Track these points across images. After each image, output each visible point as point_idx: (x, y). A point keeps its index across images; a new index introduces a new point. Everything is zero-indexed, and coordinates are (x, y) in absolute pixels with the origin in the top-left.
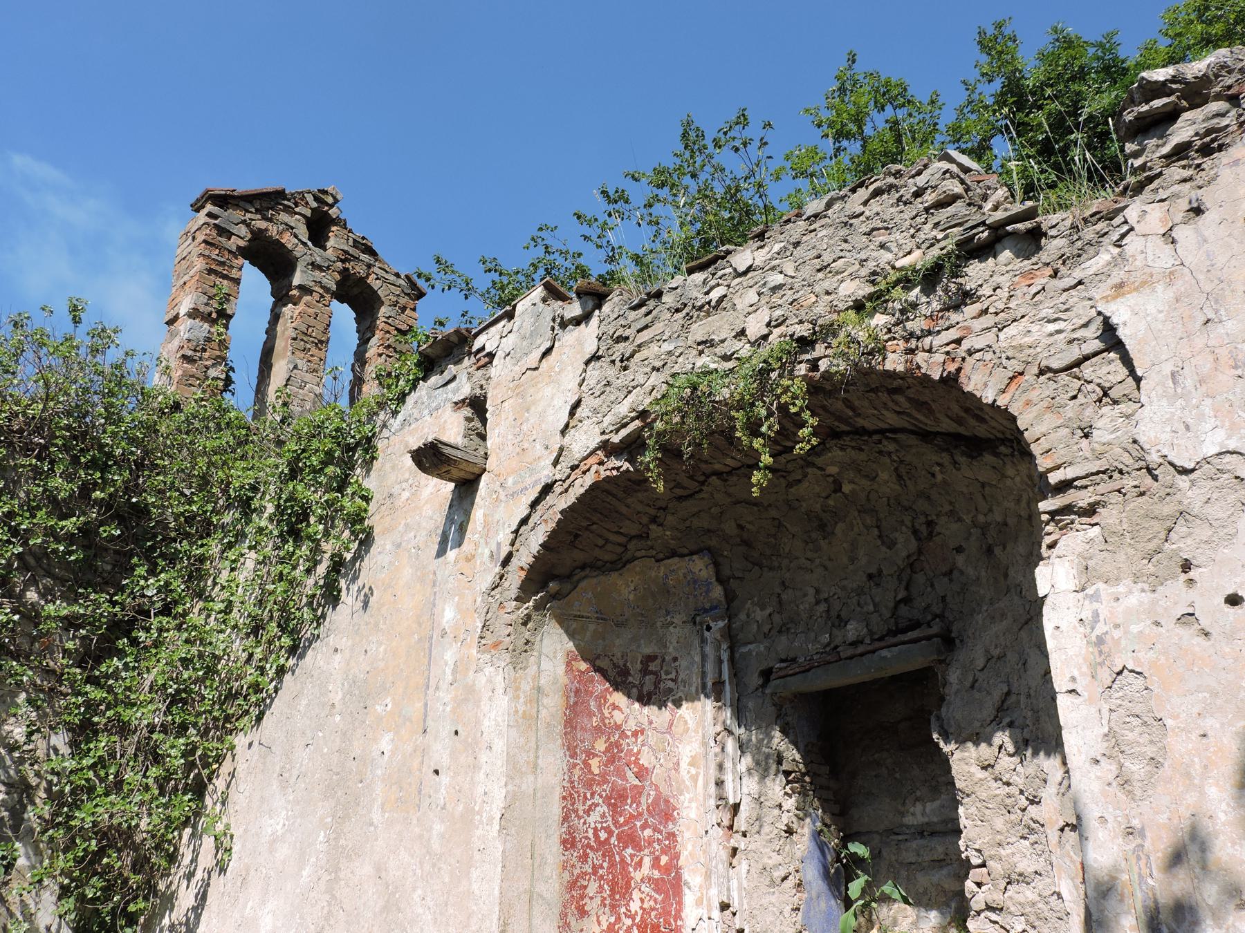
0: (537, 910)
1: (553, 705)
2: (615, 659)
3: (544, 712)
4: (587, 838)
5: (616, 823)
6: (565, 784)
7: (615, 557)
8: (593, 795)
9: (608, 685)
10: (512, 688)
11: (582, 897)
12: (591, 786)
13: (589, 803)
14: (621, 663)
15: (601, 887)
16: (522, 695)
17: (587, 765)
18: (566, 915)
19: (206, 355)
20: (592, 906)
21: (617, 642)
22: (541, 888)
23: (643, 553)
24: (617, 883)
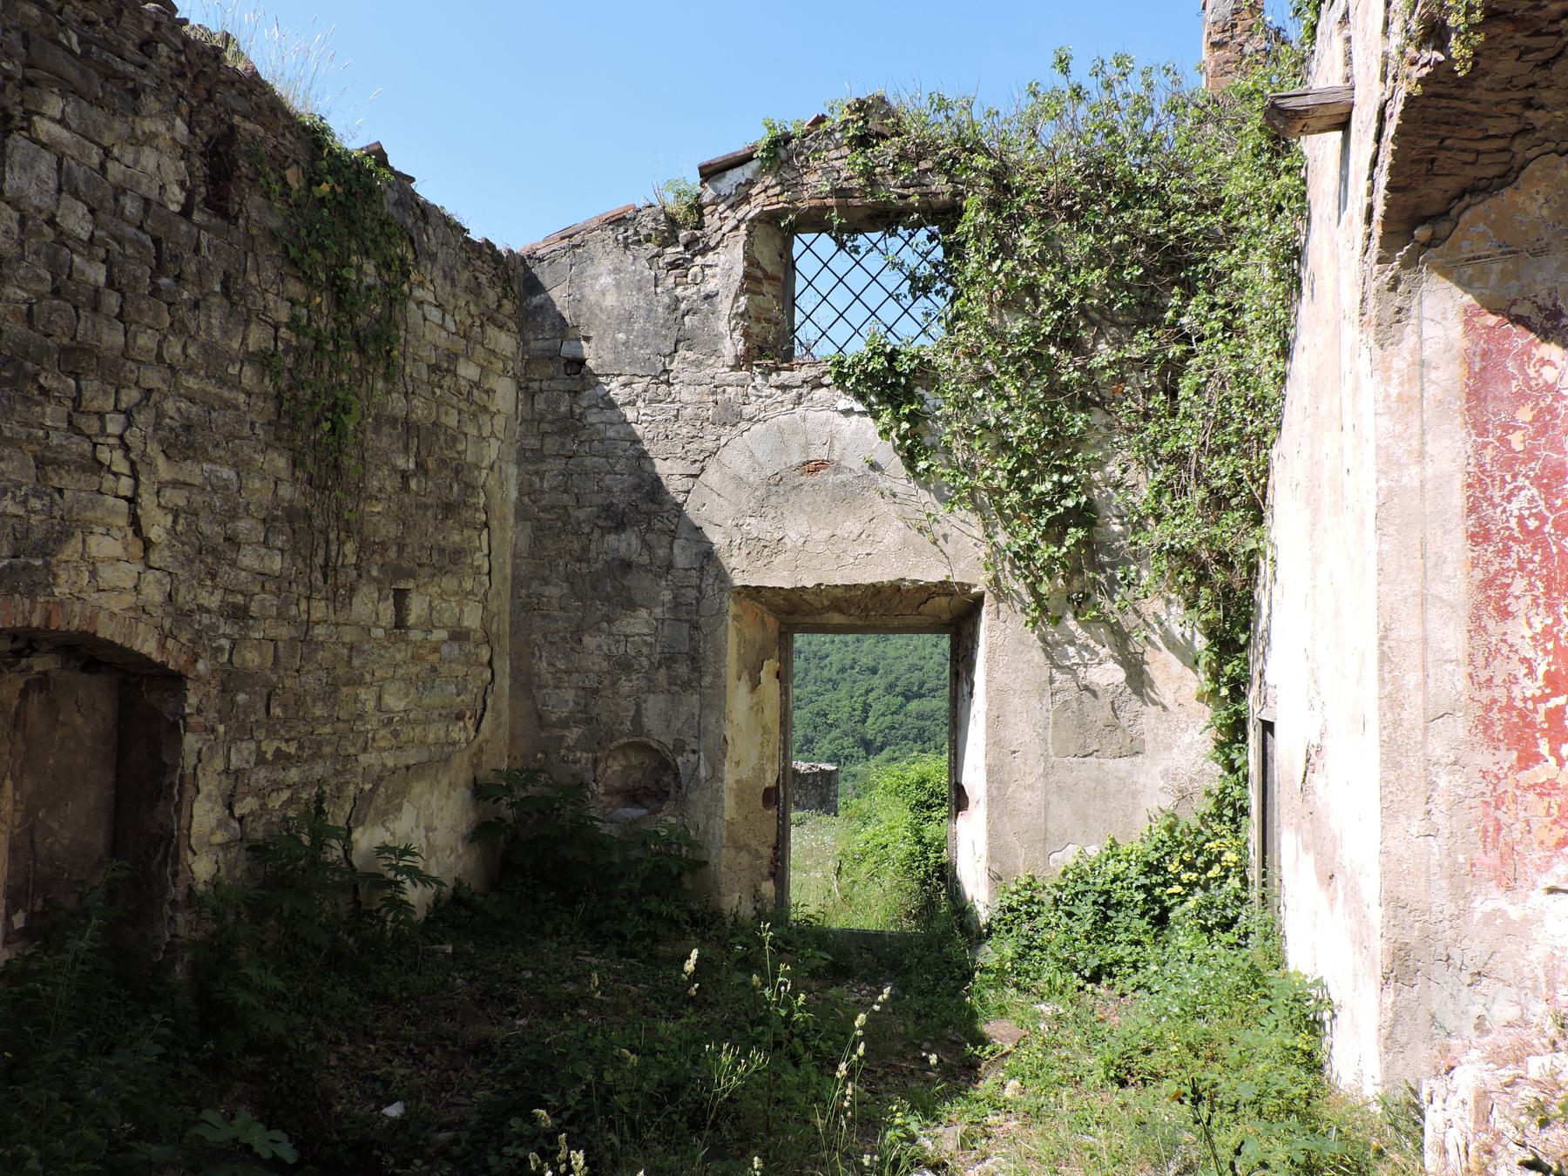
0: (1433, 613)
1: (1447, 378)
2: (1540, 301)
3: (1431, 390)
4: (1508, 528)
5: (1551, 507)
6: (1470, 469)
7: (1503, 169)
8: (1514, 477)
9: (1532, 336)
10: (1383, 370)
11: (1504, 597)
12: (1511, 466)
13: (1509, 487)
14: (1549, 304)
15: (1530, 584)
16: (1395, 375)
17: (1503, 441)
18: (1479, 618)
19: (1238, 30)
20: (1519, 606)
21: (1540, 276)
22: (1439, 589)
23: (1536, 151)
24: (1554, 579)
